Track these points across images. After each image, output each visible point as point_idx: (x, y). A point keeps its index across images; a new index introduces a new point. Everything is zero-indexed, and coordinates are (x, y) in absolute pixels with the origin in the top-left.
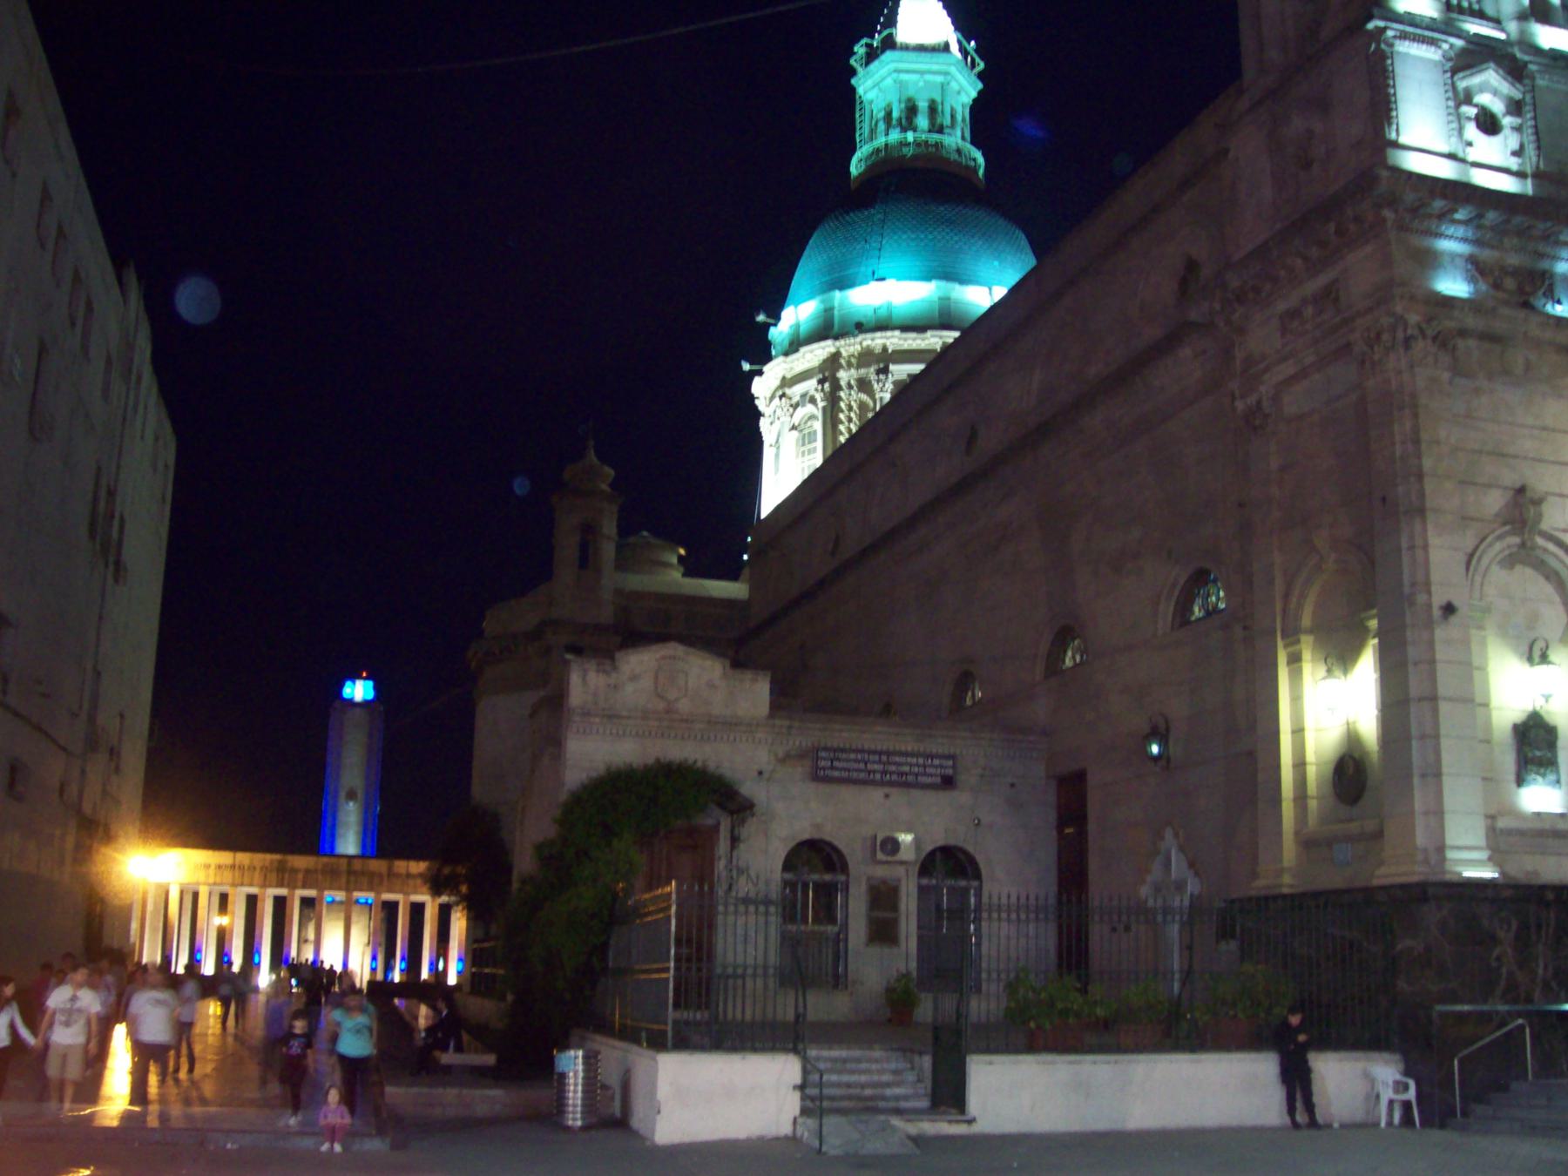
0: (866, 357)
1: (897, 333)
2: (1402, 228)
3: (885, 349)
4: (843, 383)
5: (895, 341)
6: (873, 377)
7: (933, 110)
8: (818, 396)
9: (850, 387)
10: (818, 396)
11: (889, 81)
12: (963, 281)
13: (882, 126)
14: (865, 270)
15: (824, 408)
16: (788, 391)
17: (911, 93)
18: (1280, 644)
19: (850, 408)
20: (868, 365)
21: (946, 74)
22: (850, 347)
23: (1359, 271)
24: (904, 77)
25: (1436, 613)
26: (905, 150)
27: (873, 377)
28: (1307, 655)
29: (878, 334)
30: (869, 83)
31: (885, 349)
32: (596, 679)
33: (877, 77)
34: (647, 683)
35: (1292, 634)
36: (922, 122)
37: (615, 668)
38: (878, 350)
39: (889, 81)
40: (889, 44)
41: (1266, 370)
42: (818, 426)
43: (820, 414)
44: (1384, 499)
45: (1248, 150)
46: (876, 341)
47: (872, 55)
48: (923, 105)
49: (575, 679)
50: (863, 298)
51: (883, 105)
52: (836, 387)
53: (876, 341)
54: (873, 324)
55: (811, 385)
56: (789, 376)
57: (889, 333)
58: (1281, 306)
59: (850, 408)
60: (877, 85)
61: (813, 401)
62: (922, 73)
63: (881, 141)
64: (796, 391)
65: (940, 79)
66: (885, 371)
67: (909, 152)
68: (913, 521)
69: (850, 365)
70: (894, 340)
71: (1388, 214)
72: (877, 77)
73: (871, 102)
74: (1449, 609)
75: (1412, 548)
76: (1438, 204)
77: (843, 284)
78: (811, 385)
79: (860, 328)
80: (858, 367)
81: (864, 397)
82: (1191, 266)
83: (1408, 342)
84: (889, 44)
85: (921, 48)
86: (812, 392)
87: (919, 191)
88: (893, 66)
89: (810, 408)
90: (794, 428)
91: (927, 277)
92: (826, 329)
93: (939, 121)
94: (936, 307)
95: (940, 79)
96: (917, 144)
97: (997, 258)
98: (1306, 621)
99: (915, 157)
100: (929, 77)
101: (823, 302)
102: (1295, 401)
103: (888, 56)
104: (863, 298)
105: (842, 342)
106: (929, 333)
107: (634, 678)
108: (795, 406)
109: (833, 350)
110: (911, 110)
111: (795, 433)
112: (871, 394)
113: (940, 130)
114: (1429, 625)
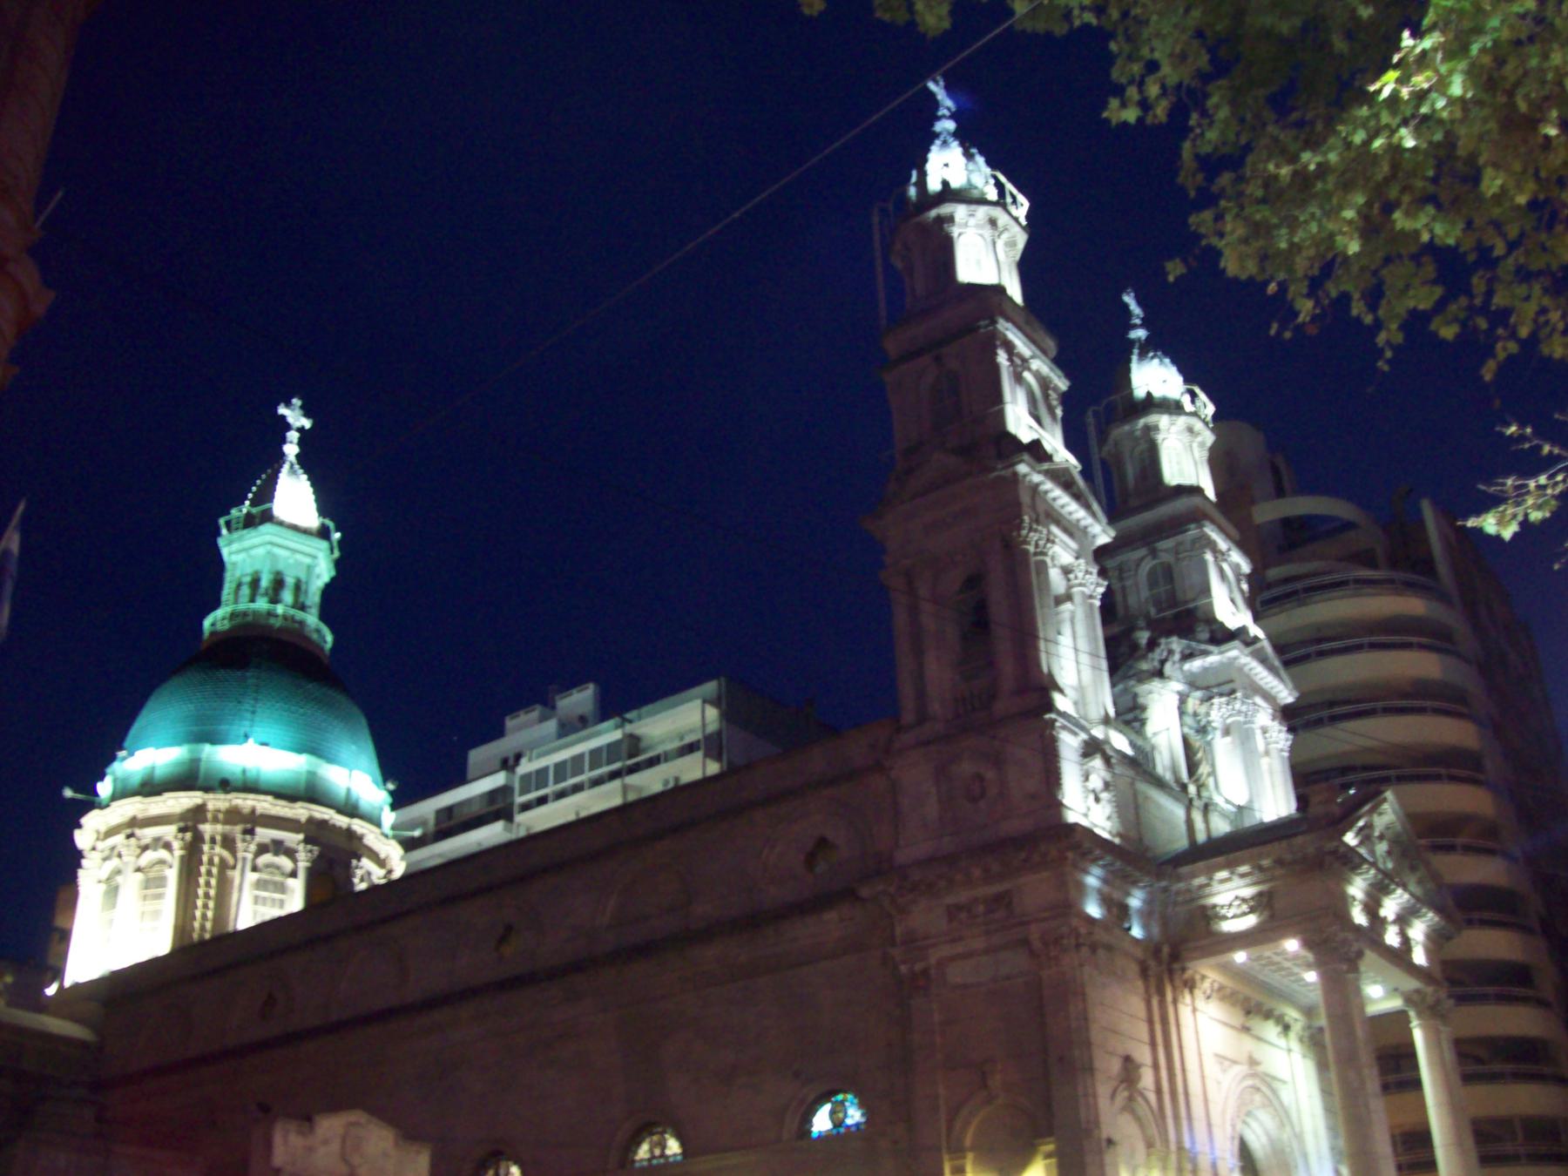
0: (233, 815)
1: (269, 798)
2: (1075, 866)
3: (253, 811)
4: (207, 837)
5: (266, 805)
6: (239, 837)
7: (298, 587)
8: (176, 845)
9: (213, 841)
10: (176, 845)
11: (261, 551)
12: (330, 760)
13: (246, 591)
14: (244, 726)
15: (182, 857)
16: (138, 832)
17: (281, 567)
18: (946, 1157)
19: (211, 862)
20: (235, 824)
21: (315, 557)
22: (217, 802)
23: (1033, 890)
24: (277, 550)
25: (1104, 1144)
26: (272, 621)
27: (239, 837)
28: (969, 1168)
29: (252, 796)
30: (235, 547)
31: (253, 811)
32: (296, 1140)
33: (246, 544)
34: (335, 1147)
35: (958, 1151)
36: (288, 596)
37: (312, 1129)
38: (246, 811)
39: (261, 551)
40: (267, 517)
41: (934, 945)
42: (172, 875)
43: (176, 864)
44: (1061, 1059)
45: (914, 775)
46: (246, 802)
47: (250, 522)
48: (290, 581)
49: (278, 1139)
50: (230, 757)
51: (249, 570)
52: (198, 838)
53: (246, 802)
54: (239, 784)
55: (169, 831)
56: (140, 816)
57: (262, 797)
58: (950, 900)
59: (211, 862)
60: (244, 553)
61: (168, 846)
62: (295, 551)
63: (243, 605)
64: (149, 833)
65: (308, 560)
66: (251, 832)
67: (277, 623)
68: (430, 1004)
69: (215, 820)
70: (265, 805)
71: (1070, 855)
72: (246, 544)
73: (234, 564)
74: (1110, 1142)
75: (1086, 1095)
76: (1098, 852)
77: (215, 739)
78: (169, 831)
79: (225, 785)
80: (226, 822)
81: (225, 854)
82: (822, 842)
83: (1078, 946)
84: (267, 517)
85: (295, 528)
86: (169, 838)
87: (264, 659)
88: (268, 538)
89: (162, 854)
90: (138, 870)
91: (300, 750)
92: (187, 779)
93: (302, 599)
94: (303, 779)
95: (308, 560)
96: (285, 617)
97: (355, 743)
98: (968, 1142)
99: (280, 629)
100: (298, 557)
101: (191, 751)
102: (957, 974)
103: (267, 528)
104: (230, 757)
105: (211, 796)
106: (299, 804)
107: (326, 1142)
108: (145, 848)
109: (199, 801)
110: (279, 583)
111: (140, 876)
112: (233, 851)
113: (303, 608)
114: (1100, 1152)
